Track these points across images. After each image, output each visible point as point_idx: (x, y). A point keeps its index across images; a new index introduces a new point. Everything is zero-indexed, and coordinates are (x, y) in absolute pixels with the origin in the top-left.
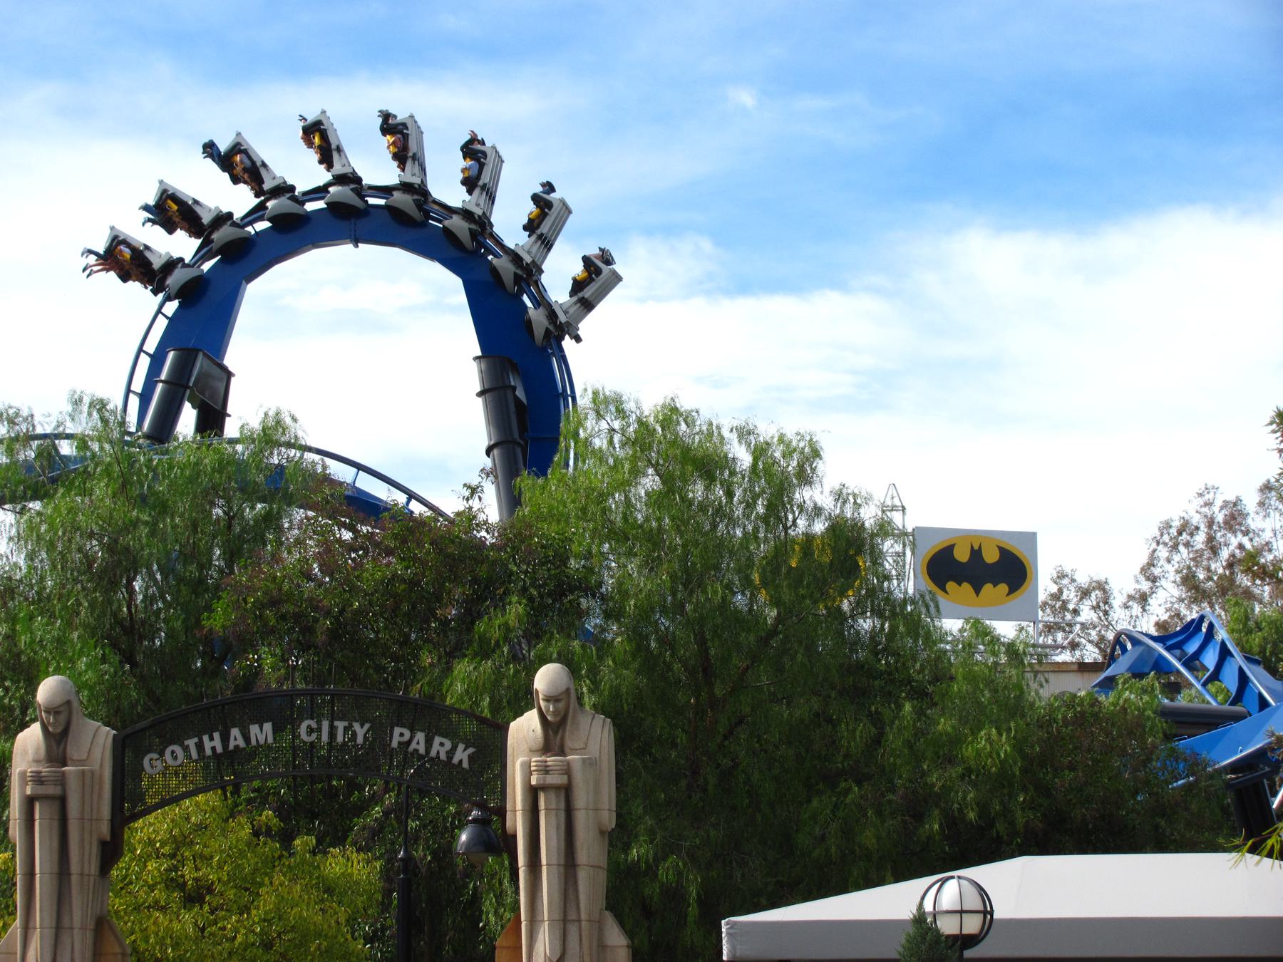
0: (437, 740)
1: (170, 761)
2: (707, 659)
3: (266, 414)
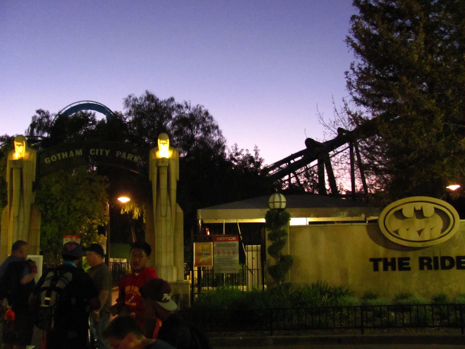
0: (129, 155)
1: (52, 160)
2: (411, 317)
3: (172, 100)
